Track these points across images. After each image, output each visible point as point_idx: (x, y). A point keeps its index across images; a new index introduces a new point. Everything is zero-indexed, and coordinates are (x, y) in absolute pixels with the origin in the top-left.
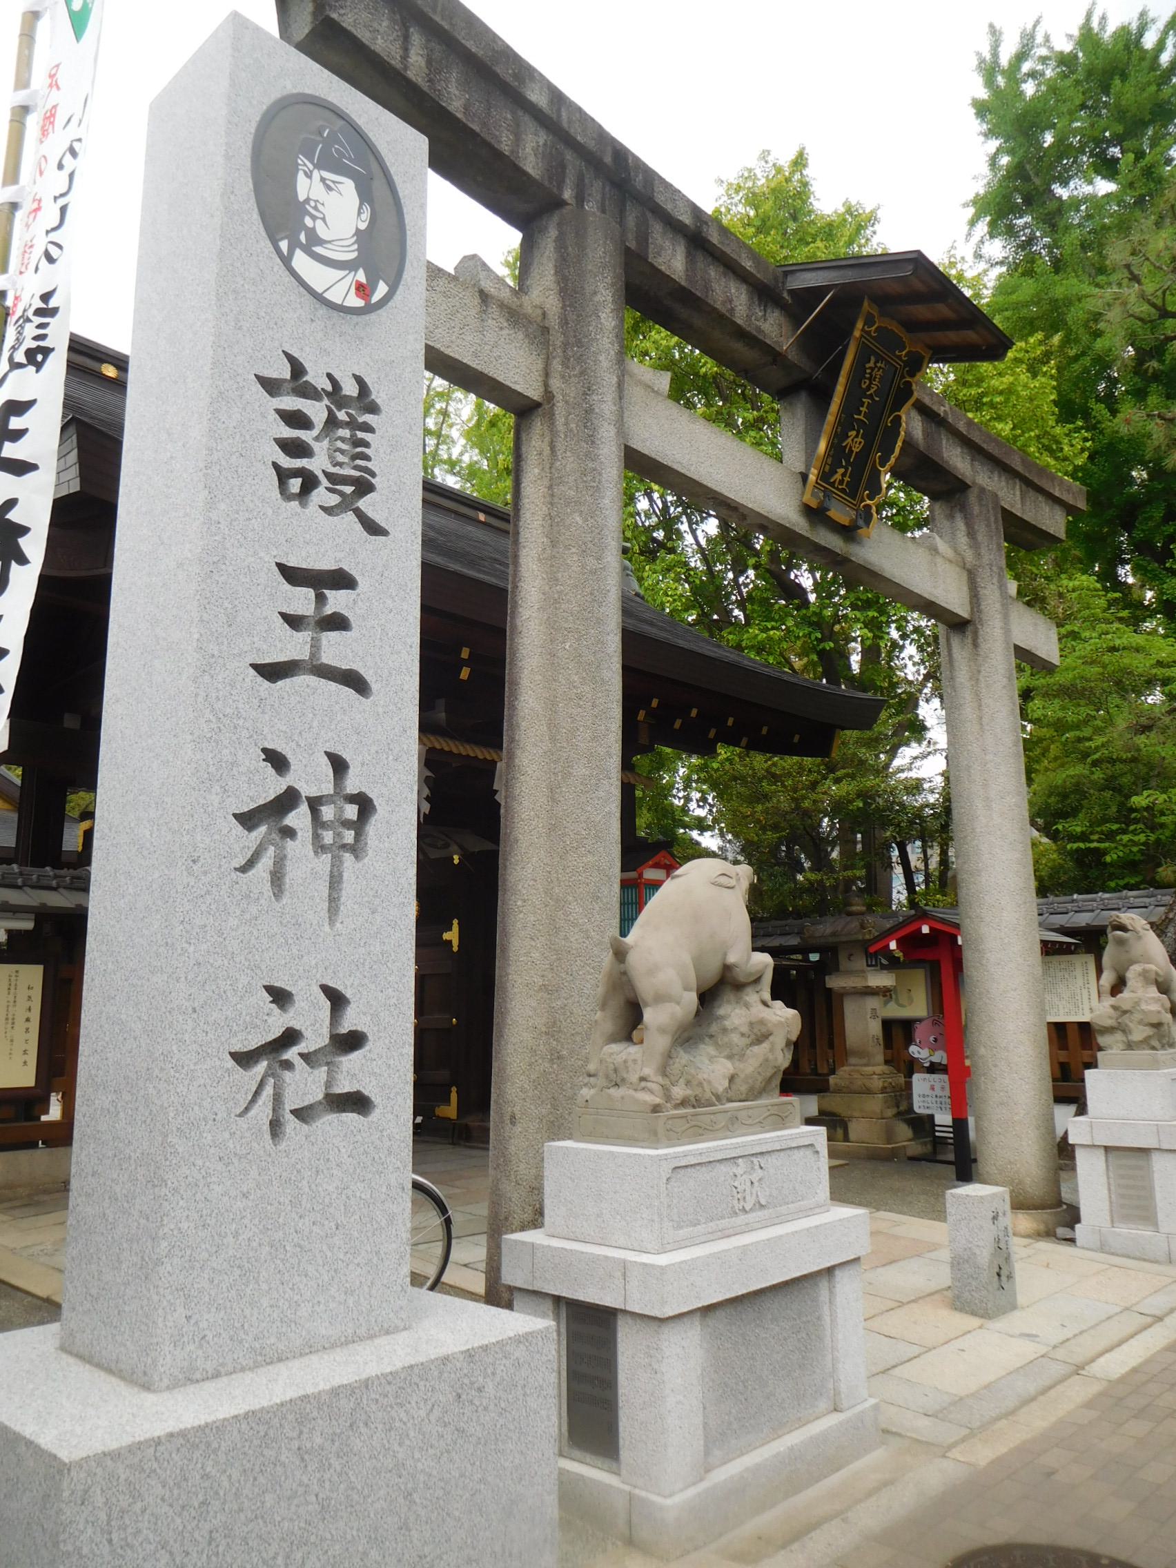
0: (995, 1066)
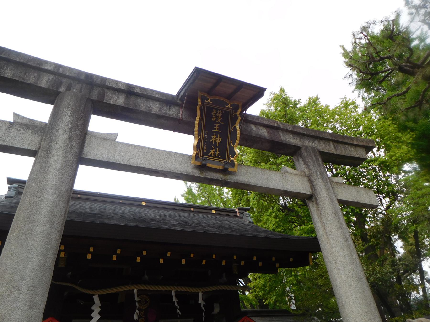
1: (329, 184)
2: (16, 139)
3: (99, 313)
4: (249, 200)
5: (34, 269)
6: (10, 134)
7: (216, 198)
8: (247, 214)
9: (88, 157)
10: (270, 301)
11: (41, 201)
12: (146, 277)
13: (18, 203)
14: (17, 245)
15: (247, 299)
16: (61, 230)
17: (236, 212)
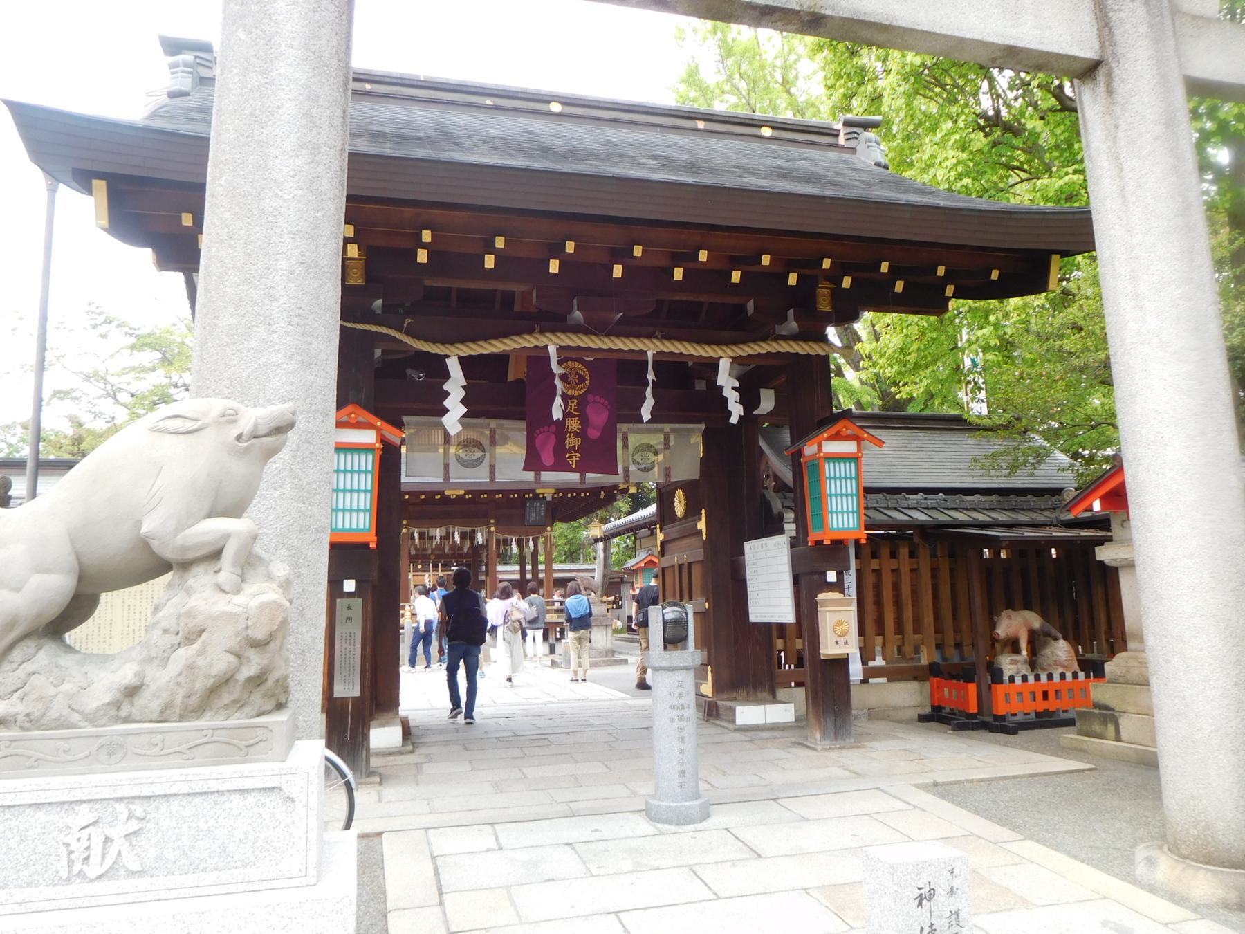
0: (1167, 661)
1: (1168, 21)
3: (463, 401)
4: (881, 95)
5: (292, 272)
7: (774, 96)
8: (869, 140)
10: (914, 390)
11: (272, 83)
12: (577, 314)
13: (207, 111)
14: (237, 209)
15: (847, 390)
16: (342, 170)
17: (836, 135)
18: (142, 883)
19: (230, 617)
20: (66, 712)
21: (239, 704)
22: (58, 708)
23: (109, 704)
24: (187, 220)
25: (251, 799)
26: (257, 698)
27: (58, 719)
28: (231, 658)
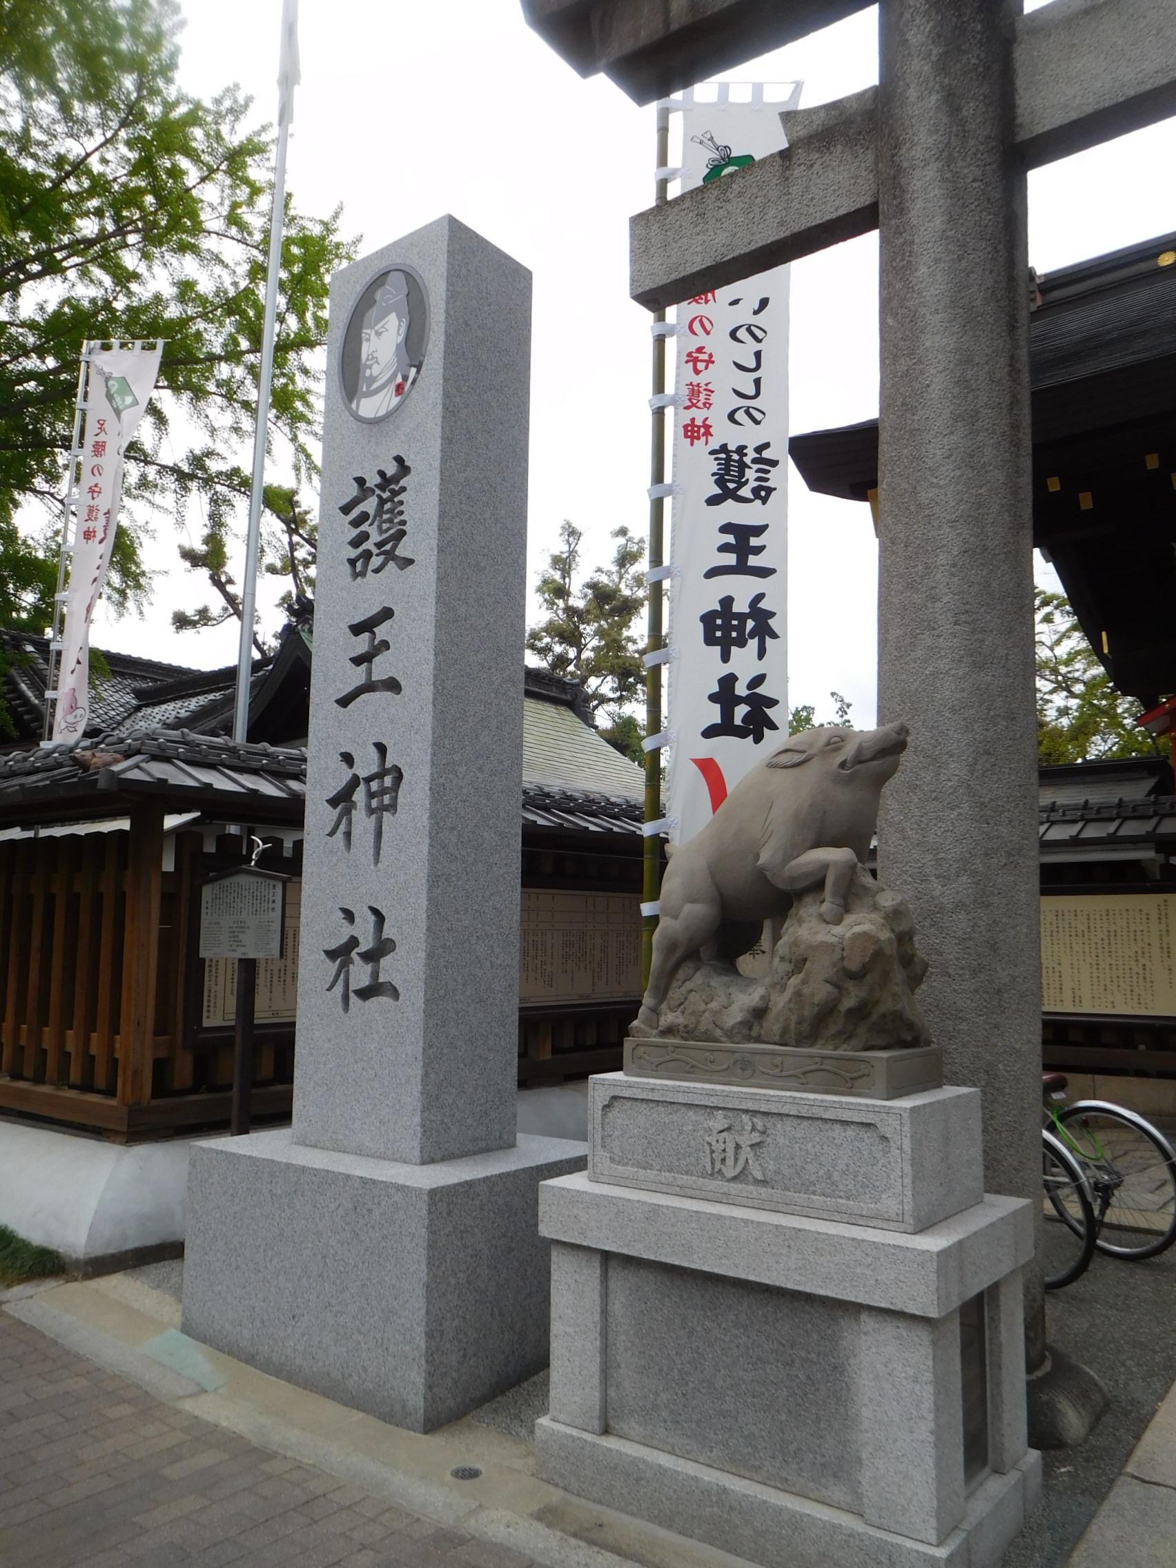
2: (813, 199)
5: (954, 566)
6: (794, 190)
9: (1040, 130)
18: (764, 1192)
19: (826, 947)
20: (711, 1026)
21: (845, 1036)
22: (705, 1023)
23: (741, 1023)
24: (1054, 485)
25: (851, 1132)
26: (862, 1030)
27: (706, 1032)
28: (830, 988)
